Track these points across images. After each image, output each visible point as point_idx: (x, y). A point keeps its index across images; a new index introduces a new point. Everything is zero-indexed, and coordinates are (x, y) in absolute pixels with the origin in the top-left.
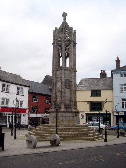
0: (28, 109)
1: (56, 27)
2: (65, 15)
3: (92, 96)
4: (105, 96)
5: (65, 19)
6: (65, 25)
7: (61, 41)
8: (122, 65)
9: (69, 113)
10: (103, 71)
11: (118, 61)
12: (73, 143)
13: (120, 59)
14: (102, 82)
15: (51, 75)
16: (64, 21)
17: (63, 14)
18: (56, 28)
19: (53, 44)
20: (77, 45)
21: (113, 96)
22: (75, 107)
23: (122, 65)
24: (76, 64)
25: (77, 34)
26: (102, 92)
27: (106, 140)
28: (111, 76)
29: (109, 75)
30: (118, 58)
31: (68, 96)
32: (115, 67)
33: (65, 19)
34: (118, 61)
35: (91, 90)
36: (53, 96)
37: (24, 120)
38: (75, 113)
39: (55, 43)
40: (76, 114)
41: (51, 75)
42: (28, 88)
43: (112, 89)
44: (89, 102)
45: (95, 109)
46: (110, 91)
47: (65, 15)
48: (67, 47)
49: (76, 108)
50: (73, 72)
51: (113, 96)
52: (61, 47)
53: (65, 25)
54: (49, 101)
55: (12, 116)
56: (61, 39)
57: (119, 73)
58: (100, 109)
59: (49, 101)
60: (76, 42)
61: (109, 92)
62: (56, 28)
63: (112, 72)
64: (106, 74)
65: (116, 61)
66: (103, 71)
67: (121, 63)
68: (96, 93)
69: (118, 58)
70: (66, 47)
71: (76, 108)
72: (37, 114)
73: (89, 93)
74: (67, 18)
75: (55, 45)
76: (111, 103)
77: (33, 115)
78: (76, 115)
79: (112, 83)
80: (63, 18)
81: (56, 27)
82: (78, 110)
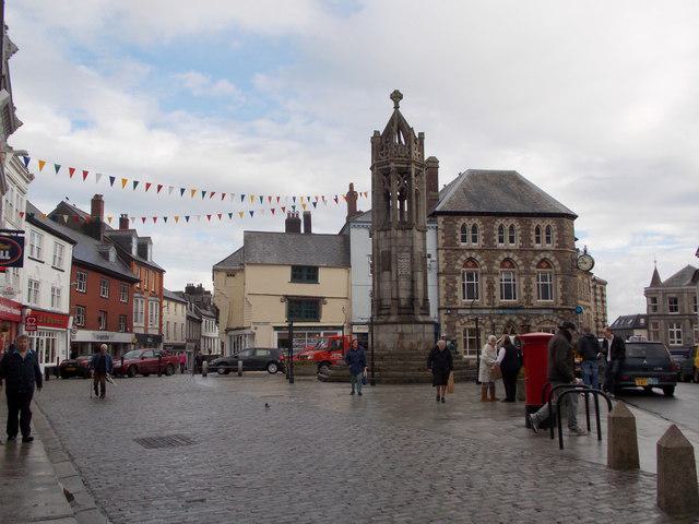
2: (397, 97)
3: (292, 281)
4: (329, 283)
5: (397, 107)
6: (398, 124)
12: (257, 376)
18: (376, 132)
21: (349, 285)
26: (323, 274)
27: (402, 335)
30: (351, 186)
33: (397, 107)
35: (293, 267)
44: (286, 296)
45: (299, 316)
47: (397, 97)
51: (349, 285)
53: (398, 124)
55: (8, 333)
58: (316, 316)
61: (340, 274)
67: (589, 236)
68: (306, 274)
69: (351, 186)
73: (288, 272)
74: (401, 103)
76: (344, 302)
77: (84, 336)
80: (392, 104)
82: (370, 281)
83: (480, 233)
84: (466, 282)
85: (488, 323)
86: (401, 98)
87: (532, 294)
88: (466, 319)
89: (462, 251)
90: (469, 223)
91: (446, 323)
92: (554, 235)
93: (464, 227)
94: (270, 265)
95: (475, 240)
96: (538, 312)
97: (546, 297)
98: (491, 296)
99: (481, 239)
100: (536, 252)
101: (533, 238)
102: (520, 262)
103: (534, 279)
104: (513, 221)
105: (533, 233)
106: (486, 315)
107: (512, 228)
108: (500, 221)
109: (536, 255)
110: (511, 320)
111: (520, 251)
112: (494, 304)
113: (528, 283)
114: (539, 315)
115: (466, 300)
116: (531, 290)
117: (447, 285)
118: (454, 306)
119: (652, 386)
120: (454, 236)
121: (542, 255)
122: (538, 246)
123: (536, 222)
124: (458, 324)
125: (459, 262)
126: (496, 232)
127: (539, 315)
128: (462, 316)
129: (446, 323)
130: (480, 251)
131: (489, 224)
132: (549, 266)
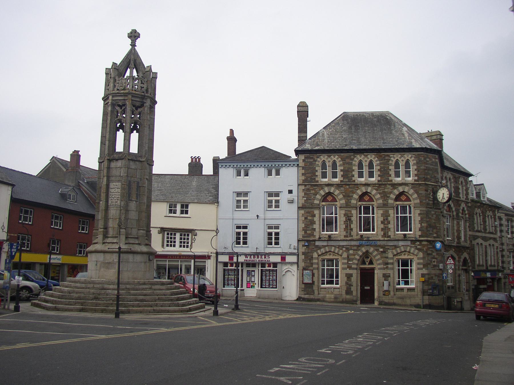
0: (7, 240)
1: (113, 63)
2: (134, 36)
5: (133, 45)
7: (126, 95)
8: (239, 150)
9: (135, 255)
10: (196, 159)
11: (232, 140)
13: (235, 135)
14: (195, 182)
15: (96, 168)
16: (131, 50)
17: (131, 33)
19: (105, 99)
20: (156, 106)
22: (147, 242)
23: (239, 150)
24: (153, 147)
25: (158, 81)
28: (211, 173)
29: (208, 169)
30: (232, 131)
31: (134, 218)
32: (223, 154)
33: (133, 45)
34: (232, 140)
36: (100, 216)
37: (70, 273)
38: (148, 255)
39: (110, 98)
40: (149, 256)
41: (96, 168)
42: (10, 188)
43: (215, 200)
46: (212, 208)
47: (134, 36)
48: (137, 109)
49: (149, 244)
50: (147, 166)
52: (123, 108)
54: (60, 223)
56: (124, 89)
57: (233, 167)
59: (60, 223)
60: (156, 100)
62: (114, 64)
63: (216, 162)
64: (201, 166)
65: (228, 138)
66: (196, 159)
69: (232, 131)
70: (134, 108)
71: (150, 245)
72: (23, 254)
74: (138, 42)
75: (110, 101)
78: (149, 260)
79: (217, 188)
80: (129, 41)
81: (113, 63)
83: (376, 169)
84: (399, 215)
85: (345, 255)
86: (139, 37)
87: (390, 226)
88: (323, 250)
89: (322, 186)
90: (329, 160)
91: (303, 253)
92: (376, 169)
93: (324, 163)
94: (159, 201)
95: (335, 175)
96: (395, 243)
97: (404, 229)
98: (348, 228)
99: (339, 174)
100: (395, 186)
101: (392, 173)
102: (378, 196)
103: (391, 212)
104: (372, 157)
105: (392, 168)
106: (343, 246)
107: (334, 164)
108: (359, 157)
109: (395, 188)
110: (367, 252)
111: (378, 186)
112: (351, 236)
113: (386, 216)
114: (396, 247)
115: (362, 232)
116: (389, 223)
117: (306, 218)
118: (312, 238)
119: (415, 328)
120: (314, 171)
121: (401, 189)
122: (399, 180)
123: (395, 157)
124: (315, 255)
125: (318, 197)
126: (356, 168)
127: (396, 247)
128: (319, 248)
129: (303, 253)
130: (338, 186)
131: (348, 160)
132: (408, 200)
